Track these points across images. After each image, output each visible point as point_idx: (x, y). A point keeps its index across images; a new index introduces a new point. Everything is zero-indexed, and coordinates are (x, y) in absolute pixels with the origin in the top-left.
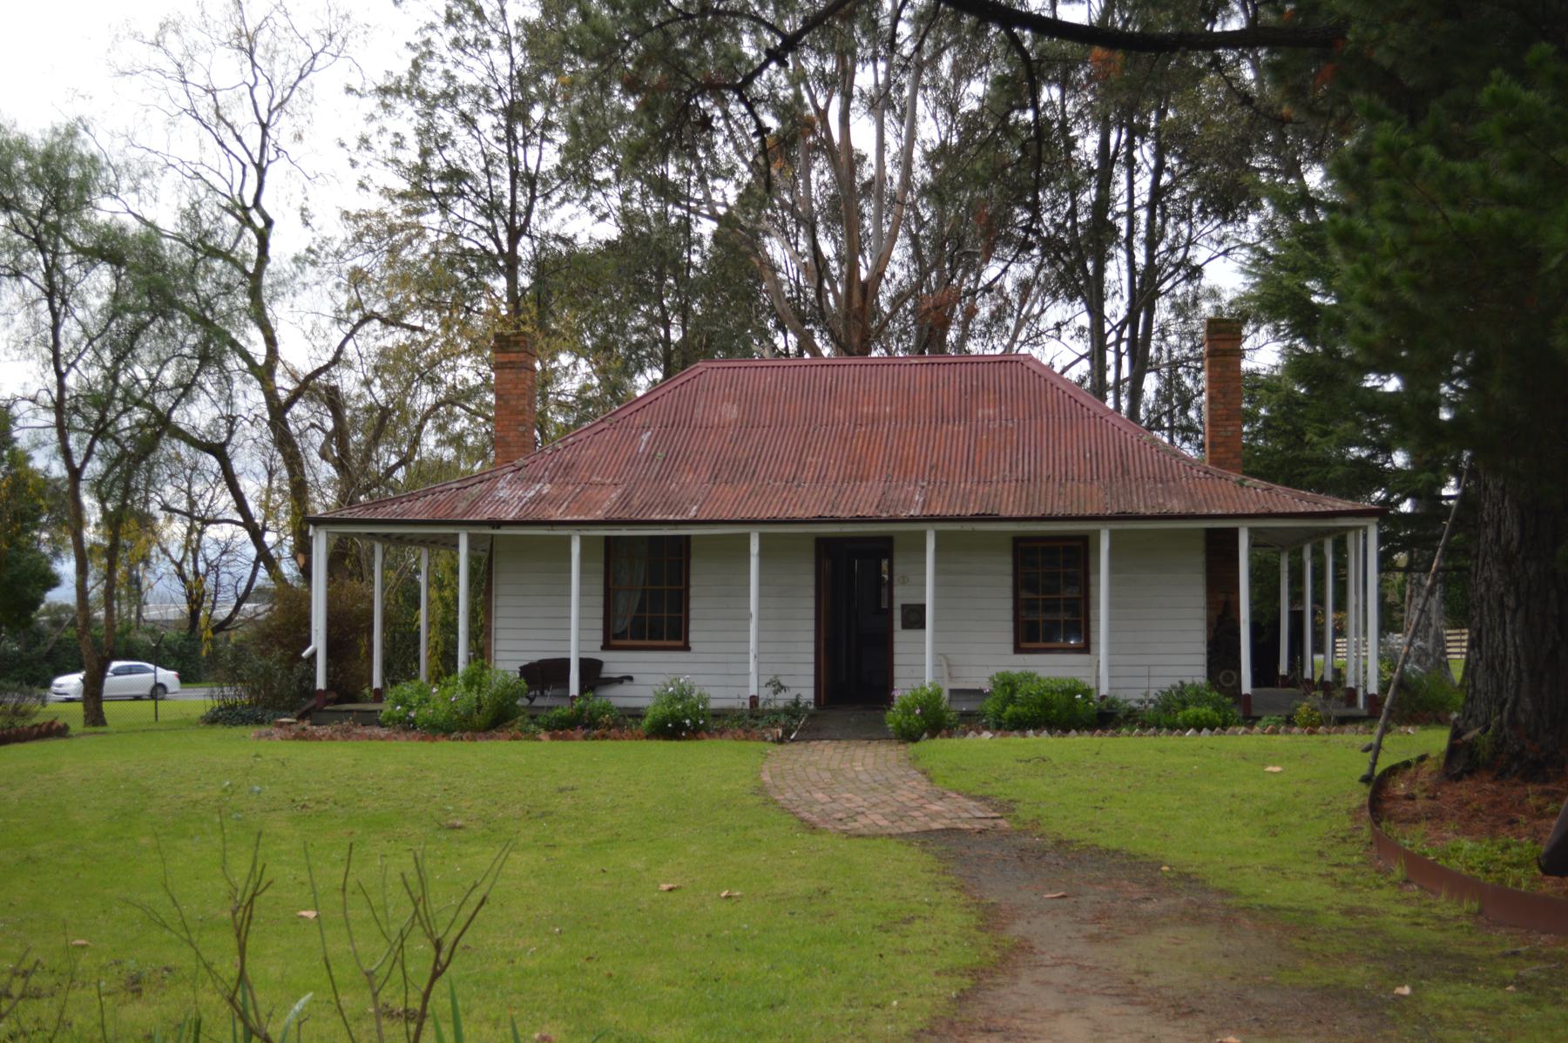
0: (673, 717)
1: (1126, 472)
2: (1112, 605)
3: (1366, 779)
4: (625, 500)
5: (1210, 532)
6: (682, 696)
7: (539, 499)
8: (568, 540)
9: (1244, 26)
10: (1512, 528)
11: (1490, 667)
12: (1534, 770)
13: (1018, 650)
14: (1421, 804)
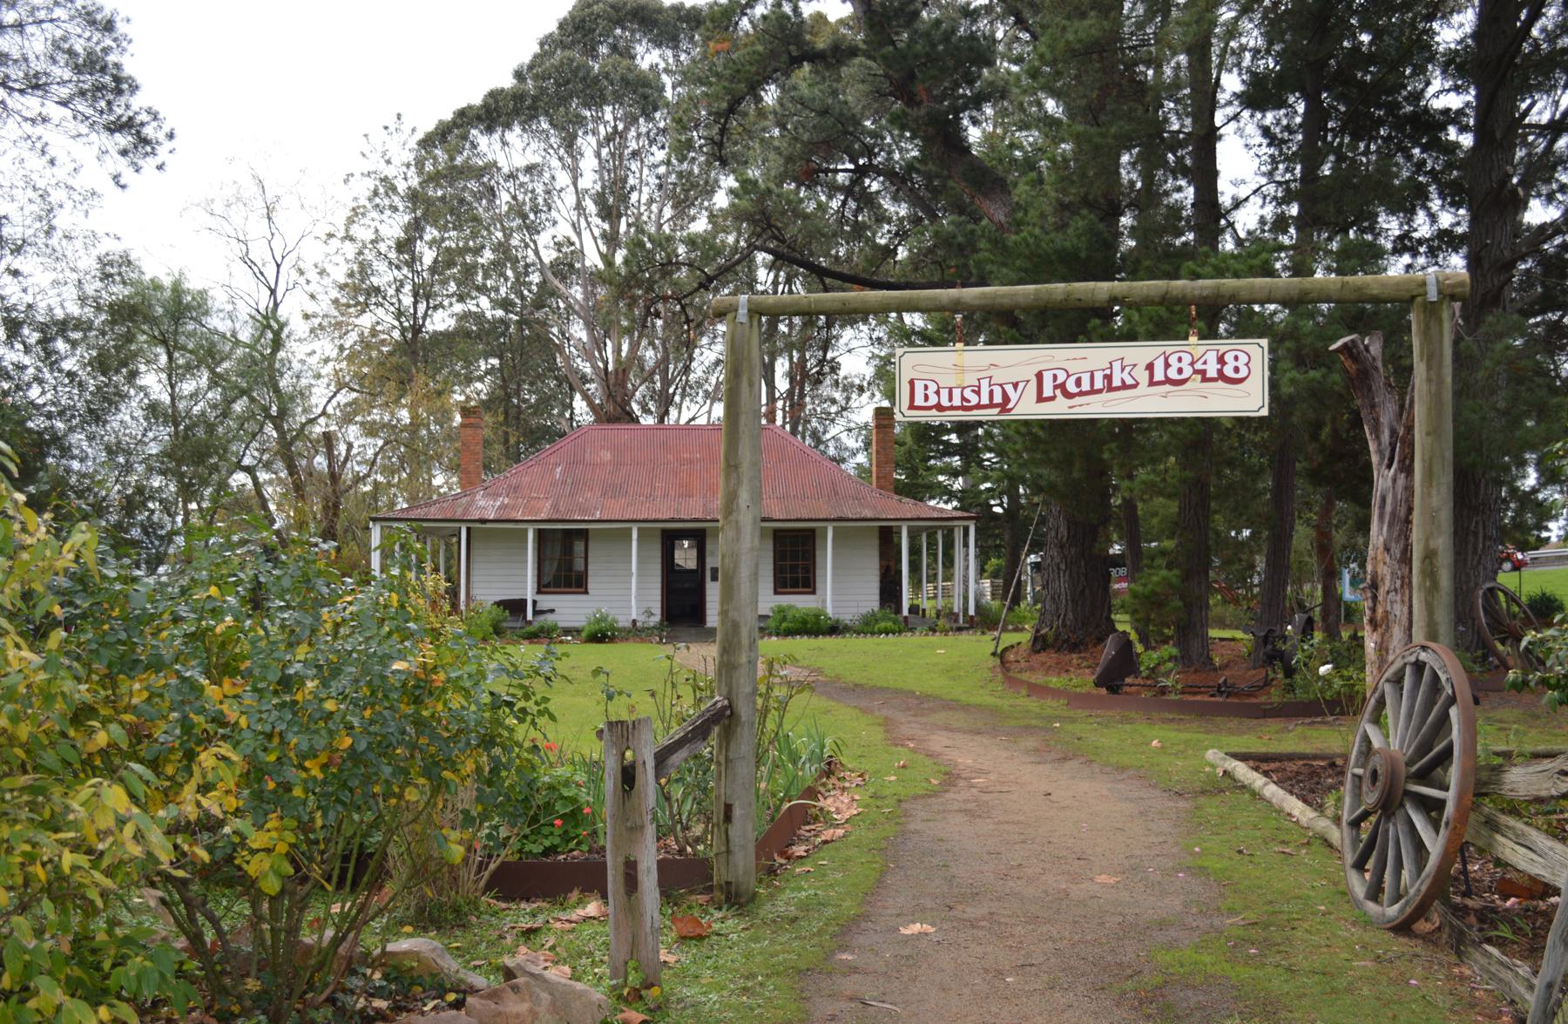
0: (600, 631)
1: (836, 494)
2: (834, 568)
3: (994, 654)
4: (555, 507)
5: (881, 528)
6: (603, 619)
7: (503, 507)
8: (526, 531)
9: (1265, 412)
10: (1063, 531)
11: (1053, 599)
12: (1074, 647)
13: (776, 593)
14: (1023, 664)
